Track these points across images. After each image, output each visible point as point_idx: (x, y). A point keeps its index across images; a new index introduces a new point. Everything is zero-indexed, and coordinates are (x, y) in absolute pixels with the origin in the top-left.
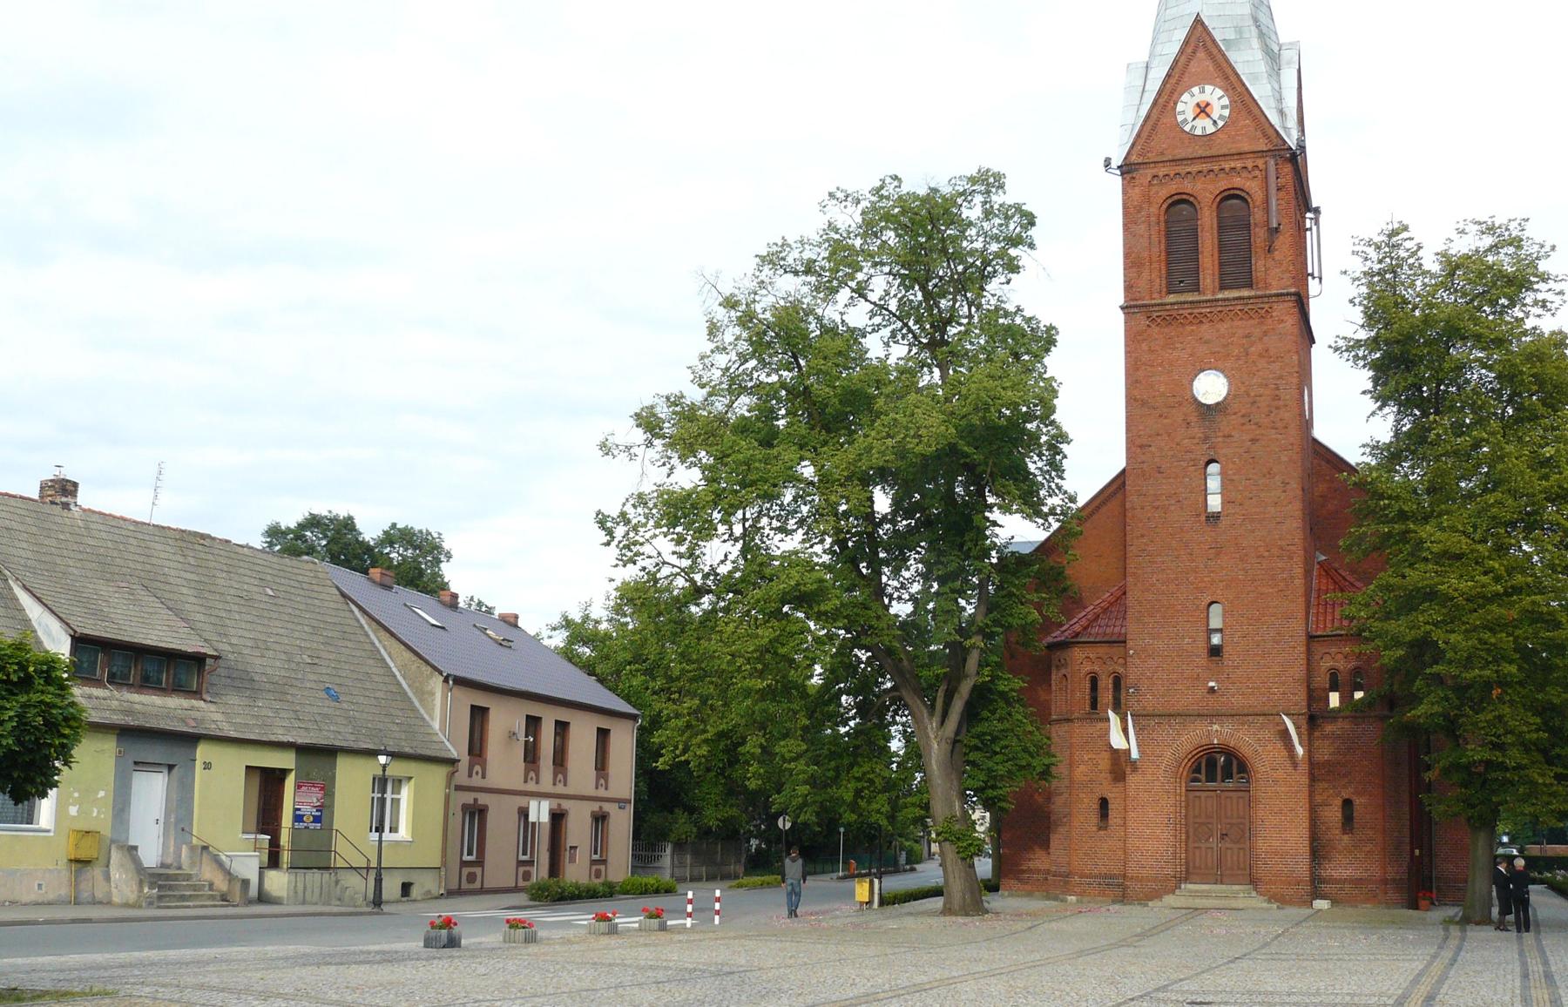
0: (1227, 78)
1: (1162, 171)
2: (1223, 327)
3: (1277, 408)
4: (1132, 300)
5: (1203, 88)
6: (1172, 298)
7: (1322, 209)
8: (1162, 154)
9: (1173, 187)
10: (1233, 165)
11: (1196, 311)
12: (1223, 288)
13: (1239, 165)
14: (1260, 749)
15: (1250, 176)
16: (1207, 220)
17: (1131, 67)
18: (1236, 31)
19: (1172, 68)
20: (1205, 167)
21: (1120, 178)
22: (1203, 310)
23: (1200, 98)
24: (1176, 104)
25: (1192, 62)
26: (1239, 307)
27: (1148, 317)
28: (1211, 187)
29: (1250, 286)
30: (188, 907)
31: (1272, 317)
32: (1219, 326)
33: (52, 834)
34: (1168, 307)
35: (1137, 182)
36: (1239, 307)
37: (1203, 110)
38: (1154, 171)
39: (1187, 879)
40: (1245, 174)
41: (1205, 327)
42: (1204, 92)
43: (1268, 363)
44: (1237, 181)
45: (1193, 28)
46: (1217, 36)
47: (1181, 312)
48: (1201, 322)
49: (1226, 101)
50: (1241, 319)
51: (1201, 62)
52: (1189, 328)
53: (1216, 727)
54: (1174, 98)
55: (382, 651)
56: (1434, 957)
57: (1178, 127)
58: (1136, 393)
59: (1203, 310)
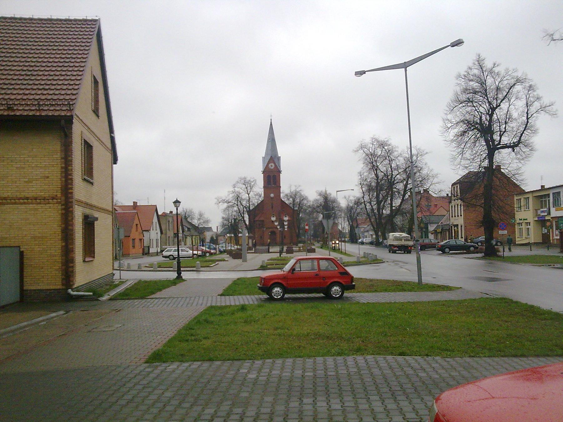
37: (272, 166)
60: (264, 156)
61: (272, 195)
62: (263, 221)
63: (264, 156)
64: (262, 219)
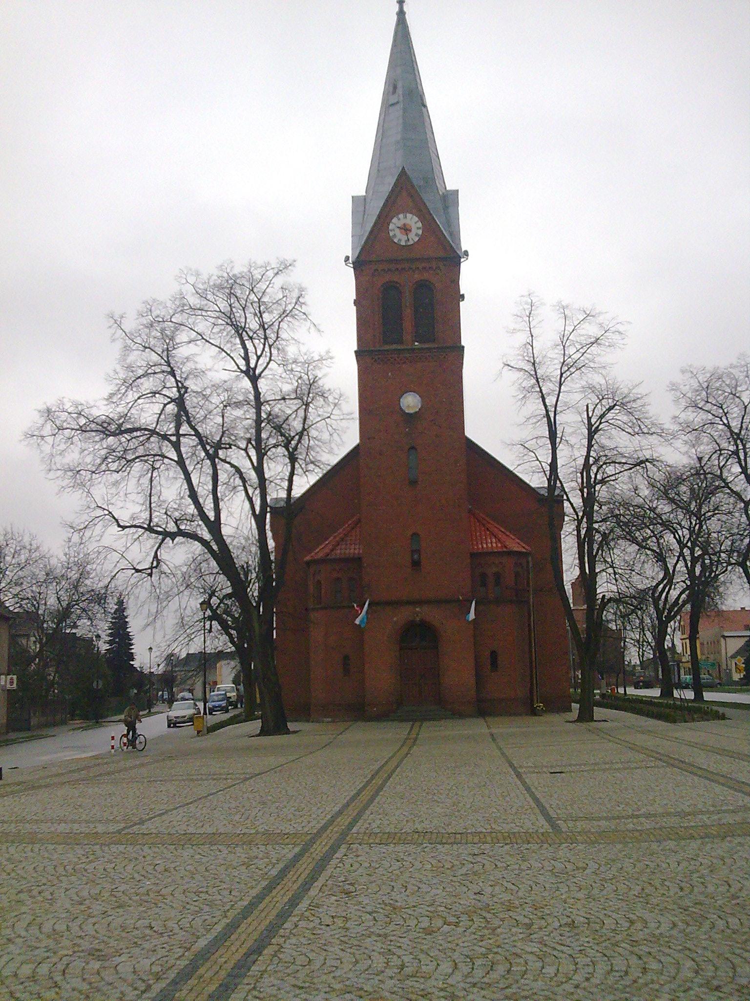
0: (420, 210)
6: (387, 347)
7: (465, 296)
9: (387, 278)
12: (386, 342)
16: (408, 299)
19: (387, 200)
21: (352, 269)
23: (408, 221)
30: (74, 724)
33: (15, 677)
37: (406, 229)
46: (415, 183)
49: (420, 225)
56: (412, 728)
57: (390, 240)
60: (363, 193)
61: (411, 402)
62: (356, 561)
63: (363, 193)
64: (353, 550)
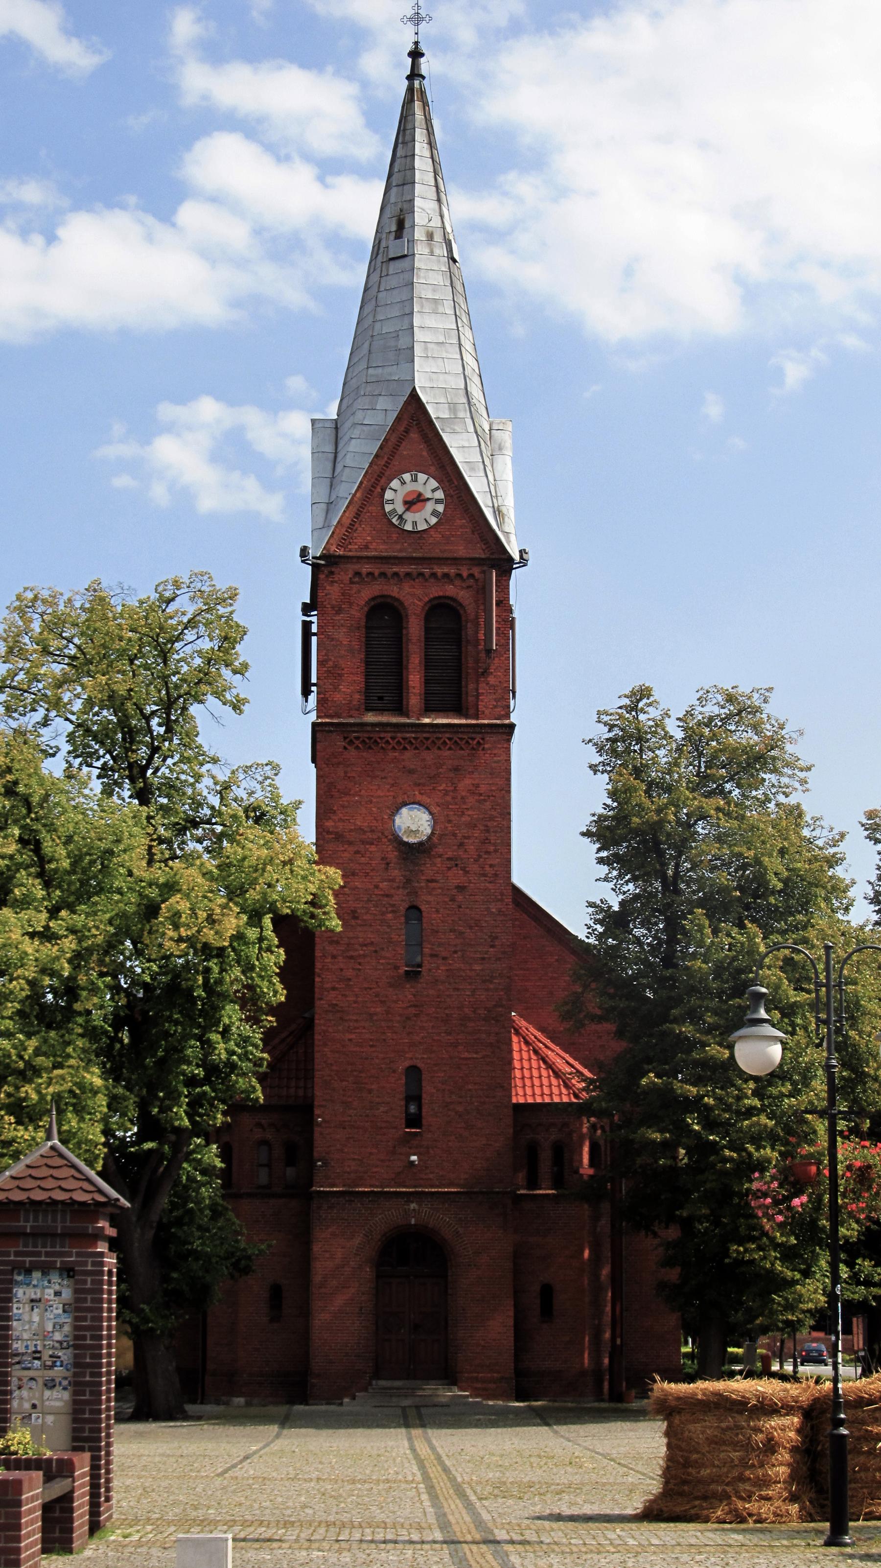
1: (365, 569)
2: (429, 757)
3: (487, 853)
4: (327, 716)
5: (416, 476)
6: (371, 718)
8: (366, 547)
10: (446, 570)
11: (399, 735)
13: (452, 571)
14: (461, 1230)
15: (464, 585)
16: (415, 628)
17: (317, 425)
18: (450, 408)
20: (412, 568)
22: (408, 735)
24: (383, 490)
25: (404, 443)
26: (448, 735)
27: (345, 738)
28: (419, 592)
29: (458, 709)
31: (483, 749)
32: (425, 754)
34: (369, 728)
35: (336, 577)
36: (448, 735)
38: (357, 567)
39: (377, 1374)
40: (458, 582)
41: (408, 755)
42: (416, 481)
43: (479, 801)
44: (450, 590)
45: (407, 403)
47: (382, 735)
48: (405, 748)
50: (450, 749)
51: (414, 445)
52: (392, 754)
53: (413, 1206)
54: (383, 481)
55: (607, 1318)
58: (329, 824)
59: (408, 735)
